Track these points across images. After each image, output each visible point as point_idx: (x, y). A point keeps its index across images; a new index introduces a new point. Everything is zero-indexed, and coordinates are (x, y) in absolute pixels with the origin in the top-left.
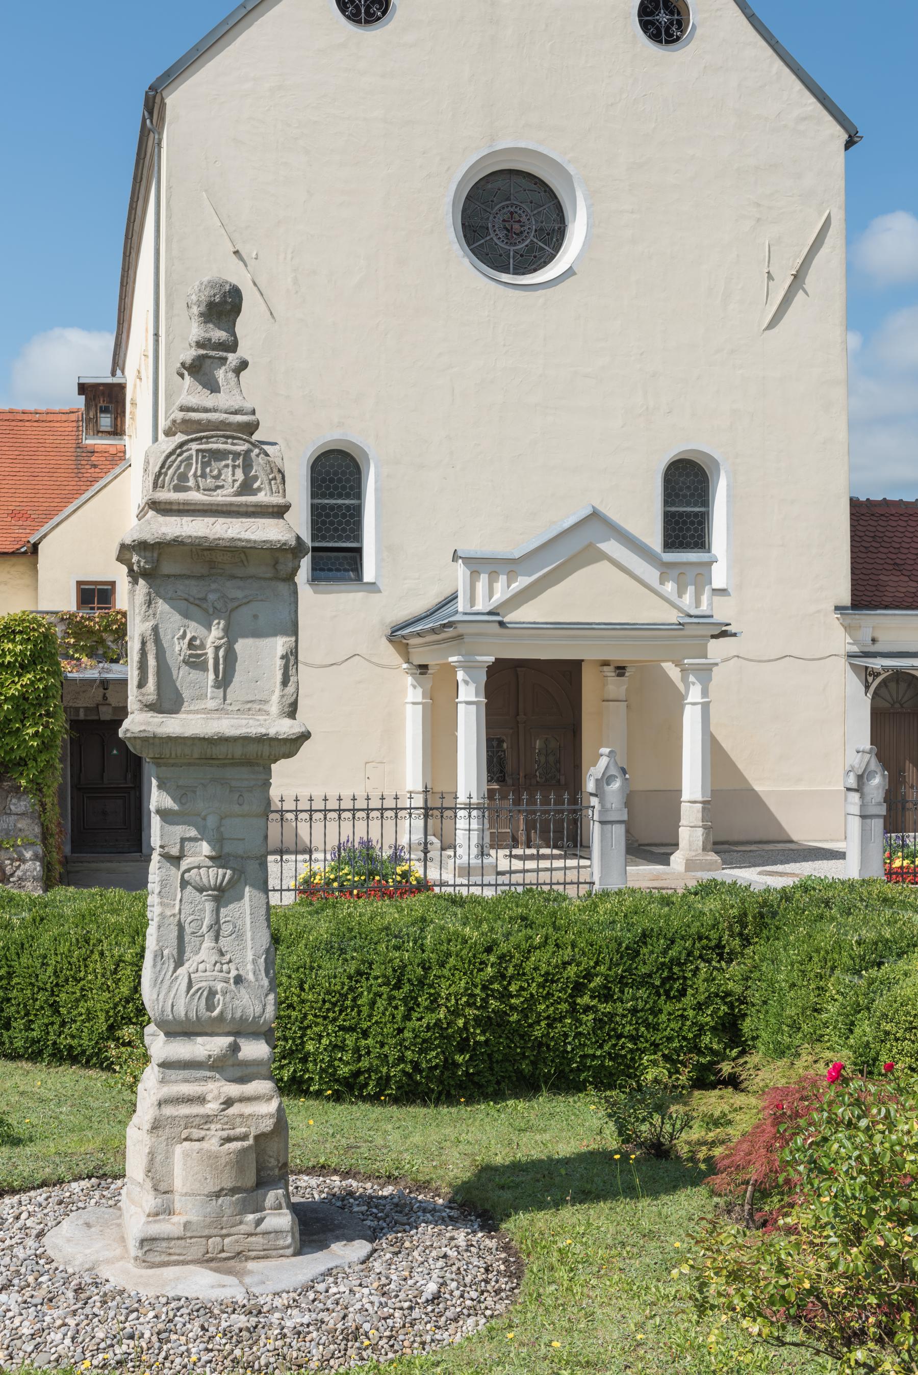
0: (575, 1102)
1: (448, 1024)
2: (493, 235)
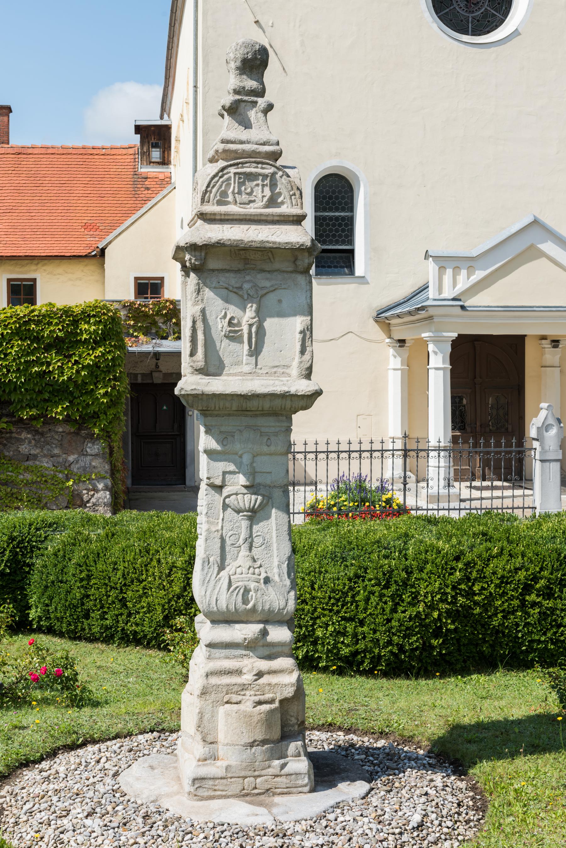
0: (524, 676)
1: (426, 615)
2: (455, 5)
